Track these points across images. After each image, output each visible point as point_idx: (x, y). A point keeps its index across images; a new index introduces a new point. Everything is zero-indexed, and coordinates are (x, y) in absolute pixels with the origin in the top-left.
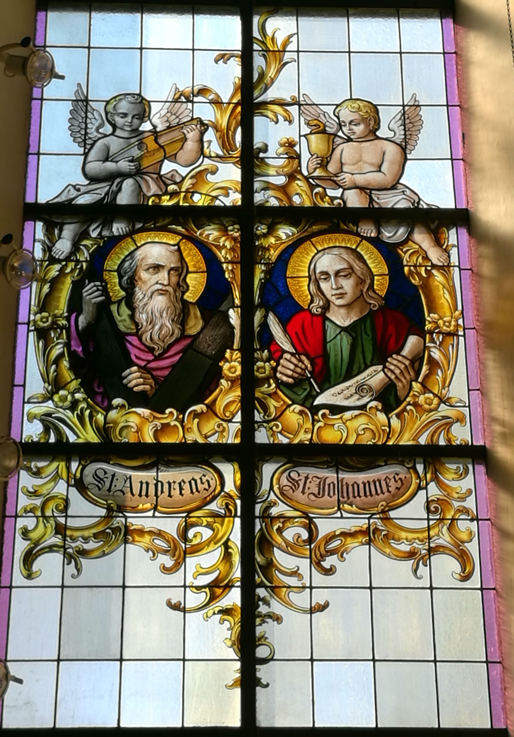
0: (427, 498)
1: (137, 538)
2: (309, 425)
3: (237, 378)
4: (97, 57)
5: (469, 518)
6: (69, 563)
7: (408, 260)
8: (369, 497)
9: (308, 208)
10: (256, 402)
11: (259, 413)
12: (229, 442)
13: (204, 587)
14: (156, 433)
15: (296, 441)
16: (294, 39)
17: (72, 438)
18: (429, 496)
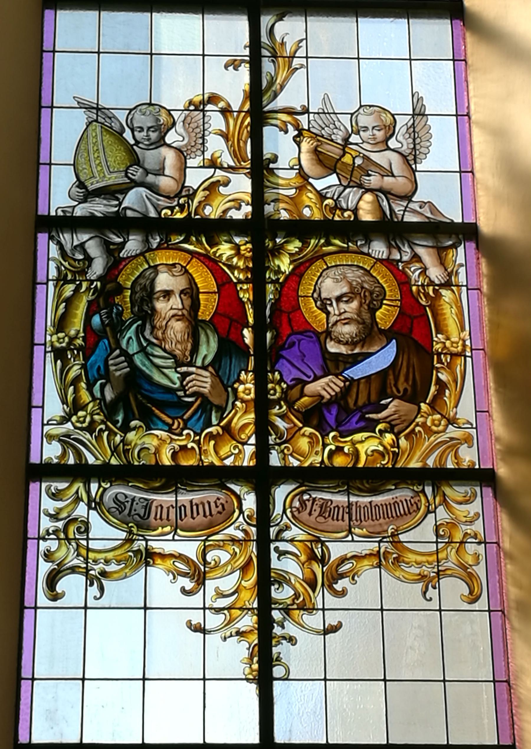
1: (159, 561)
2: (319, 448)
4: (91, 63)
5: (477, 541)
6: (92, 584)
7: (417, 279)
9: (320, 221)
12: (245, 464)
13: (224, 609)
14: (174, 455)
15: (306, 465)
17: (91, 460)
18: (438, 519)
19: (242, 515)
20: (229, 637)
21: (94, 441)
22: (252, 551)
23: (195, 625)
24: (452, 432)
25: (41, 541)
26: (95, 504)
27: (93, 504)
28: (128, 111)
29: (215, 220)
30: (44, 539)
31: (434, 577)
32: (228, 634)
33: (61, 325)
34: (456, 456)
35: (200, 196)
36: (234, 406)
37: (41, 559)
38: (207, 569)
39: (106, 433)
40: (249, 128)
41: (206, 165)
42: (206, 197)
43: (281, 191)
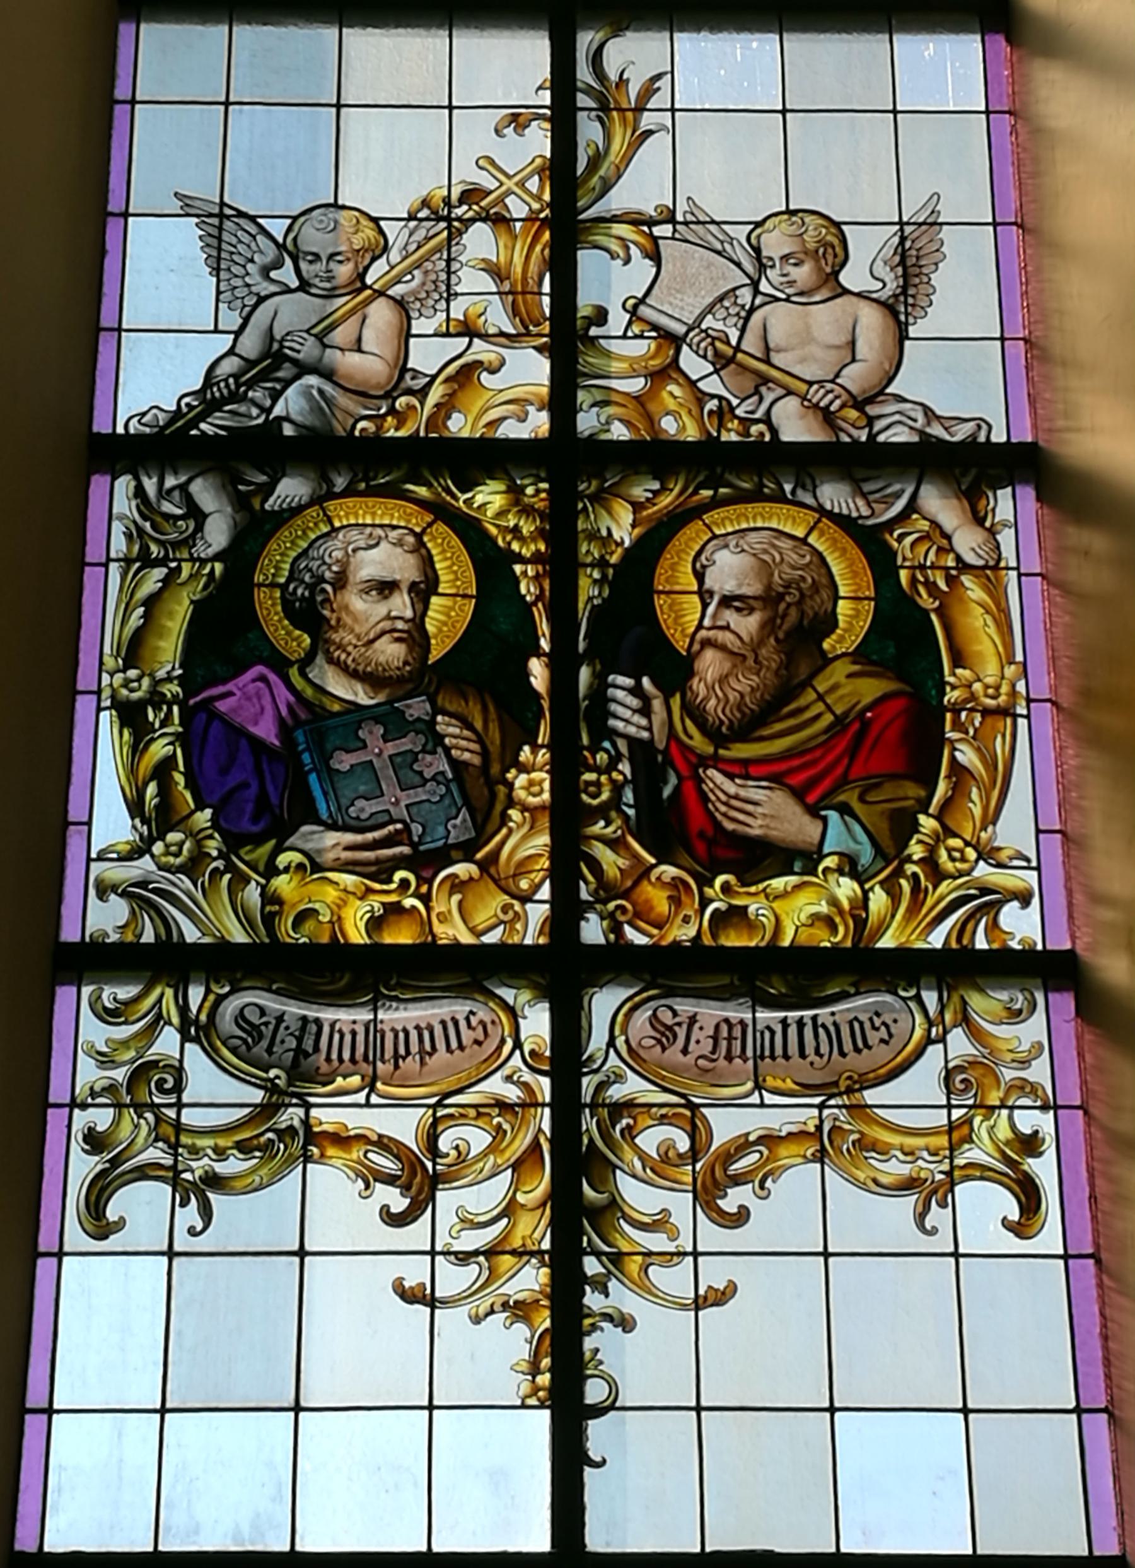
0: (946, 1062)
1: (331, 1151)
3: (542, 807)
4: (208, 126)
5: (1039, 1103)
8: (457, 1052)
12: (528, 941)
13: (476, 1253)
14: (375, 924)
17: (191, 934)
18: (950, 1057)
19: (518, 1053)
21: (199, 896)
22: (540, 1130)
23: (412, 1288)
26: (194, 1030)
27: (193, 1031)
28: (289, 221)
30: (84, 1106)
31: (941, 1183)
33: (133, 652)
34: (995, 924)
35: (435, 395)
36: (504, 819)
39: (228, 876)
41: (452, 330)
43: (614, 384)
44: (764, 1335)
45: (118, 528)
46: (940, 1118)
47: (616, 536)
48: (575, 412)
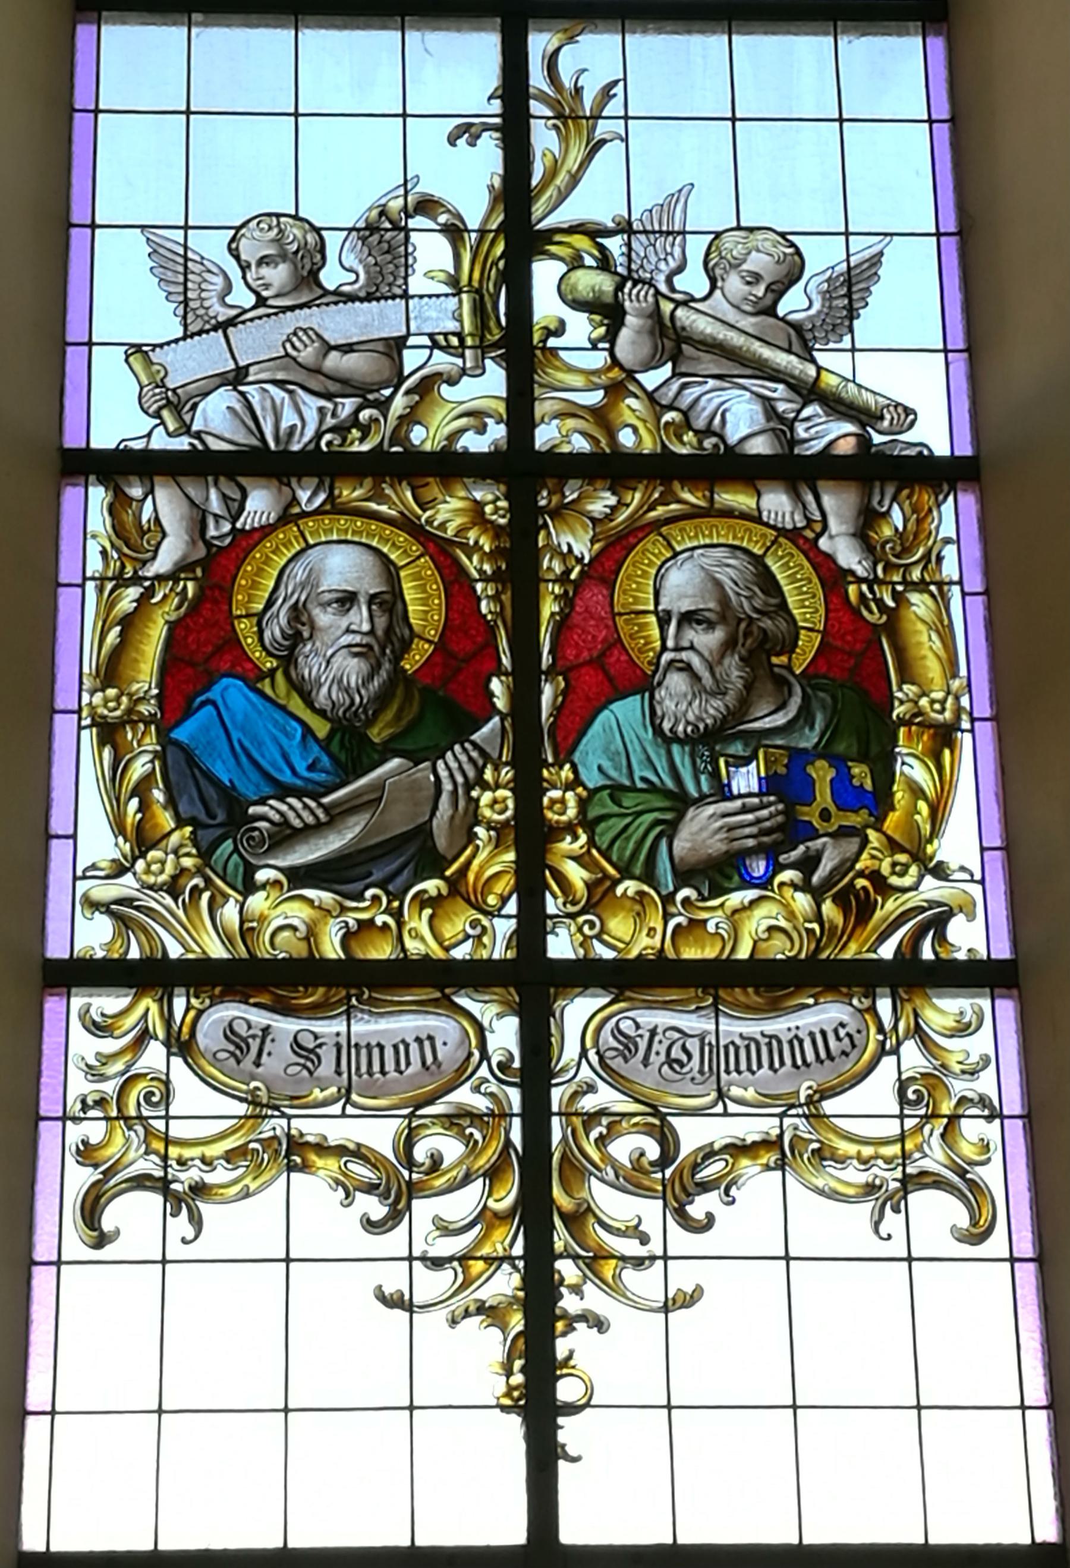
0: (900, 1073)
3: (506, 824)
5: (986, 1112)
10: (547, 873)
11: (555, 897)
12: (496, 956)
13: (451, 1259)
14: (347, 938)
15: (634, 954)
16: (619, 89)
17: (175, 951)
18: (903, 1069)
19: (485, 1063)
20: (464, 1318)
21: (180, 913)
23: (392, 1295)
24: (931, 888)
25: (69, 1123)
26: (182, 1045)
29: (432, 454)
30: (75, 1119)
31: (897, 1191)
32: (460, 1312)
33: (111, 672)
37: (70, 1160)
38: (415, 1176)
39: (206, 896)
40: (501, 264)
42: (412, 408)
44: (732, 1332)
45: (93, 549)
46: (892, 1128)
47: (577, 552)
48: (534, 426)
